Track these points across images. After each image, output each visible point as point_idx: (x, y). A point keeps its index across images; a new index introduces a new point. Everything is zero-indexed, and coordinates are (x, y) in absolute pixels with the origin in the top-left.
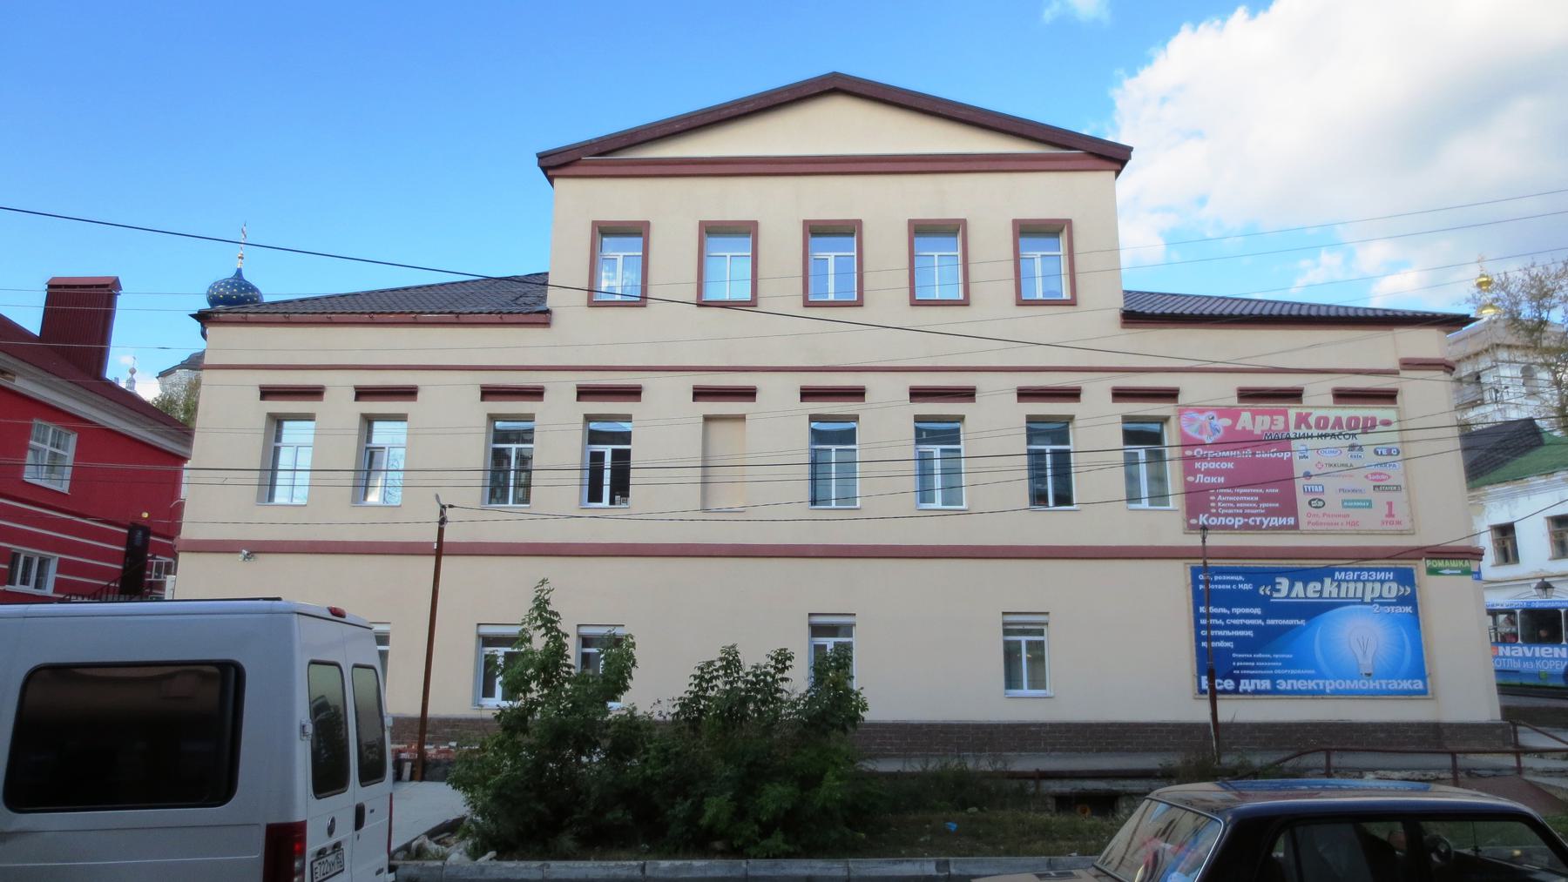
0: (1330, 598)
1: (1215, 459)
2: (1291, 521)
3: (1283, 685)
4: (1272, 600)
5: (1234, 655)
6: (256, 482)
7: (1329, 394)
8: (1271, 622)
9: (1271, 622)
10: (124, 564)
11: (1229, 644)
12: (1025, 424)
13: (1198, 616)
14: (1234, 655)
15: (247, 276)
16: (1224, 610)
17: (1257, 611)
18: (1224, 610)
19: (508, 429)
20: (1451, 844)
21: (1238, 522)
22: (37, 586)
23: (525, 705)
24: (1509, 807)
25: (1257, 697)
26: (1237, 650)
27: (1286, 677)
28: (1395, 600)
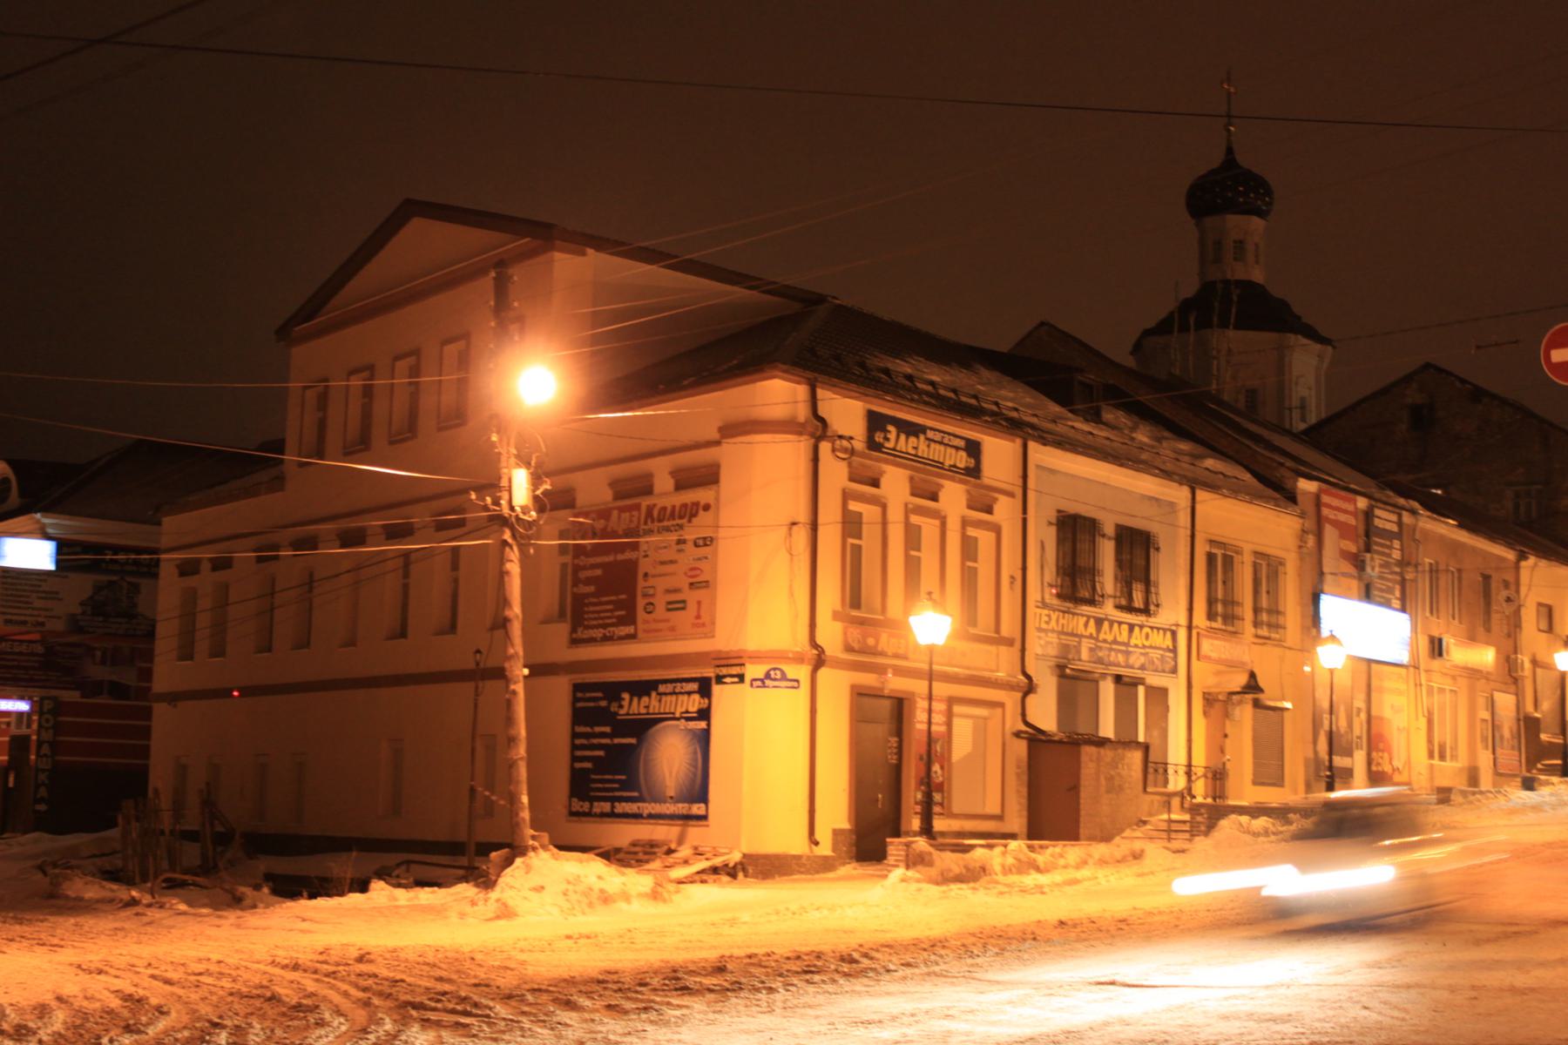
0: (639, 714)
1: (25, 615)
2: (578, 765)
3: (621, 807)
4: (619, 717)
5: (593, 777)
6: (720, 530)
7: (837, 523)
8: (617, 741)
9: (617, 741)
10: (10, 755)
11: (588, 765)
12: (722, 533)
13: (575, 735)
14: (593, 777)
15: (1244, 160)
16: (588, 729)
17: (607, 729)
18: (588, 729)
19: (67, 517)
20: (987, 959)
21: (598, 633)
22: (1152, 801)
23: (62, 1009)
24: (1215, 896)
25: (652, 821)
26: (595, 771)
27: (621, 799)
28: (695, 715)
